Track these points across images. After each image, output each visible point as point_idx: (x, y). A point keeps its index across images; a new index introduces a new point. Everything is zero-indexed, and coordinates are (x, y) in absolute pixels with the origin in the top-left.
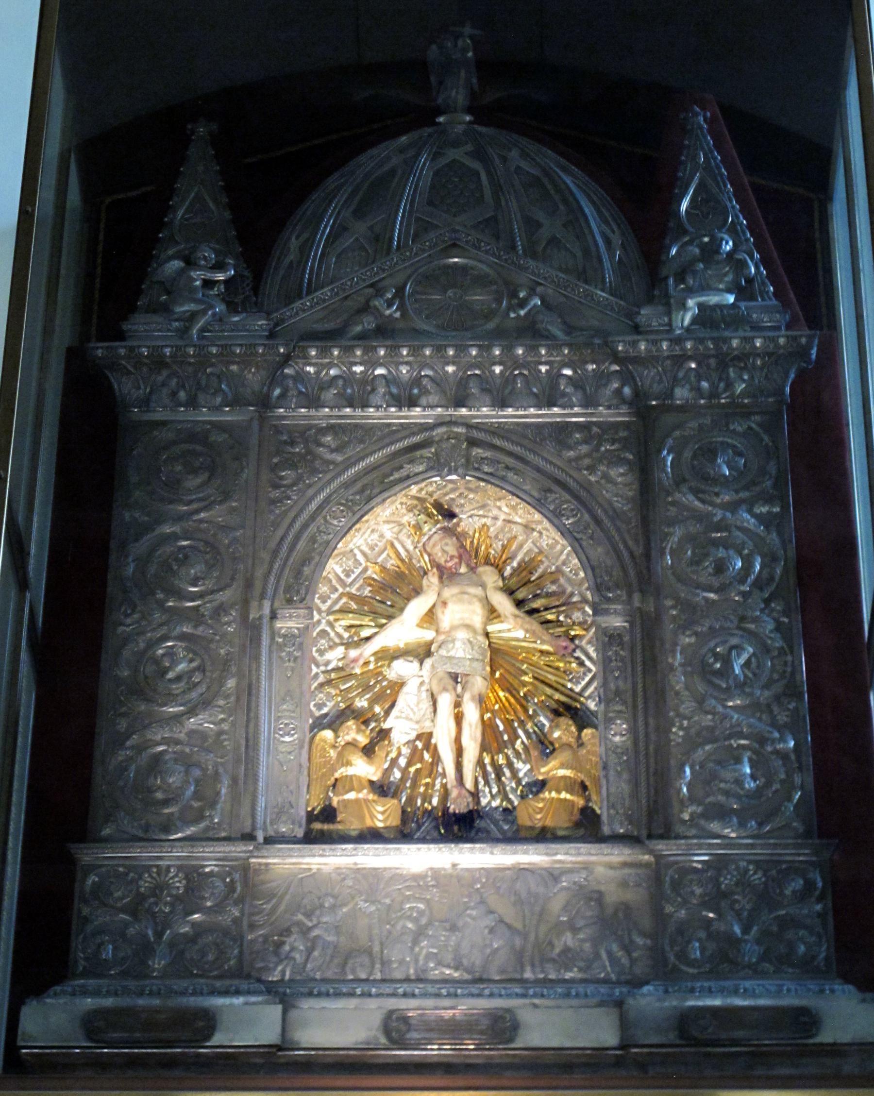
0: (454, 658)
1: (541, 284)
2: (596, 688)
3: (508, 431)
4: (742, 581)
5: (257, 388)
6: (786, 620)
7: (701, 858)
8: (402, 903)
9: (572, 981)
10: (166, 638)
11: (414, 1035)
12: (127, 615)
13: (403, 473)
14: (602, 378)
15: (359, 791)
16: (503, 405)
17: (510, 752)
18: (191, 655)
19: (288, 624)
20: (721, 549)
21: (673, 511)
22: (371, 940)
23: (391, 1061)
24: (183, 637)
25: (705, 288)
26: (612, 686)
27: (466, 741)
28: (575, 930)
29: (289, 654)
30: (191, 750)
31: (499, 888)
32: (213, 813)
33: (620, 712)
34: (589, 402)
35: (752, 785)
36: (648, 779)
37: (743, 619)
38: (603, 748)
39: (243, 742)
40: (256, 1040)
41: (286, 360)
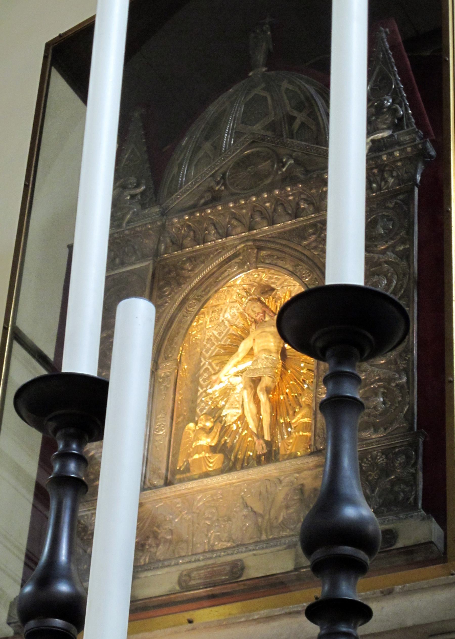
5: (152, 246)
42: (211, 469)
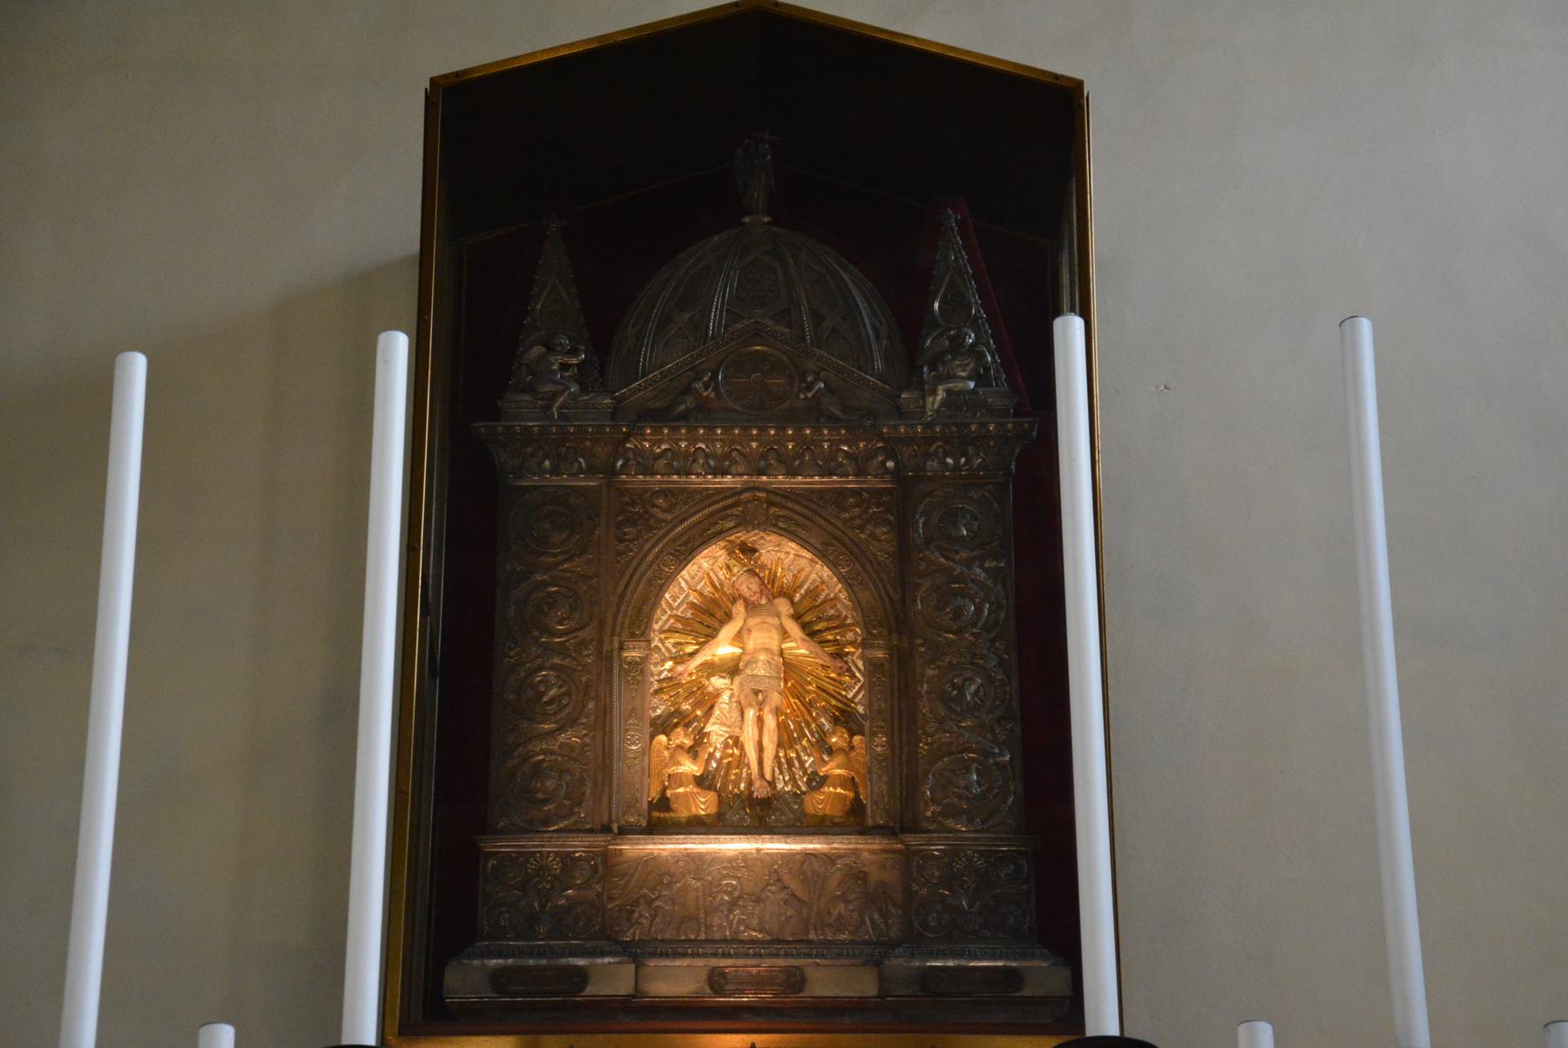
0: (757, 676)
1: (825, 370)
2: (863, 696)
3: (798, 495)
4: (974, 625)
6: (1006, 657)
7: (936, 849)
8: (720, 880)
9: (843, 942)
10: (541, 668)
11: (730, 987)
12: (511, 649)
13: (718, 528)
14: (871, 455)
15: (686, 787)
16: (795, 474)
17: (798, 747)
18: (560, 682)
19: (632, 654)
20: (959, 599)
21: (923, 566)
22: (698, 909)
23: (713, 1005)
24: (554, 668)
25: (951, 377)
26: (876, 707)
27: (766, 742)
28: (848, 902)
29: (633, 678)
30: (563, 760)
31: (791, 869)
32: (581, 810)
33: (882, 727)
34: (861, 472)
35: (978, 790)
36: (901, 784)
37: (974, 656)
38: (868, 757)
39: (601, 752)
40: (617, 991)
41: (627, 437)
42: (703, 813)
